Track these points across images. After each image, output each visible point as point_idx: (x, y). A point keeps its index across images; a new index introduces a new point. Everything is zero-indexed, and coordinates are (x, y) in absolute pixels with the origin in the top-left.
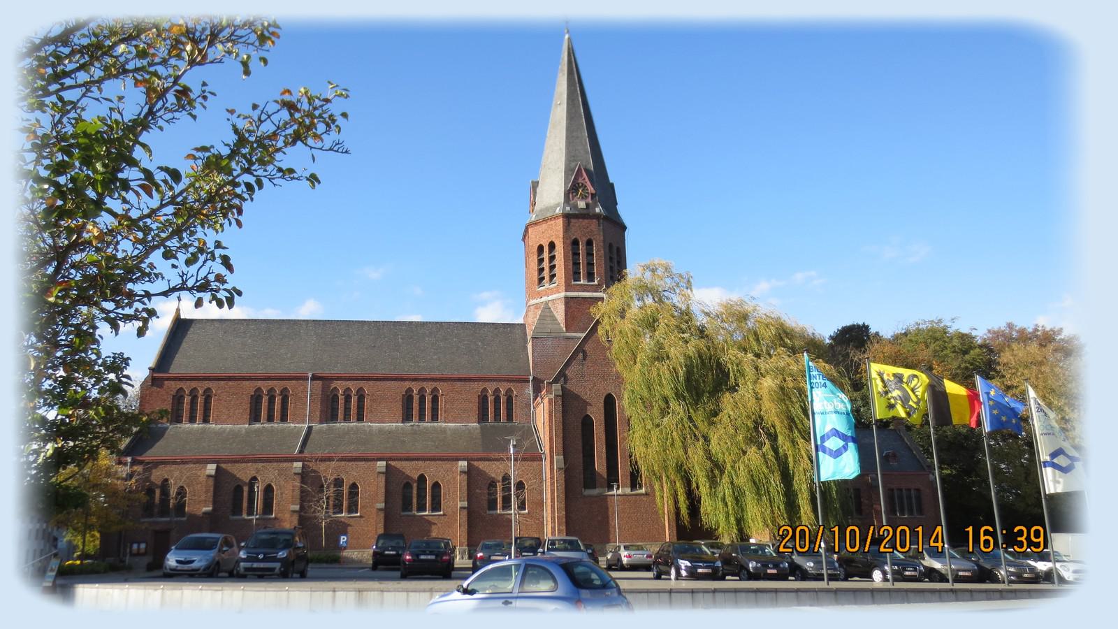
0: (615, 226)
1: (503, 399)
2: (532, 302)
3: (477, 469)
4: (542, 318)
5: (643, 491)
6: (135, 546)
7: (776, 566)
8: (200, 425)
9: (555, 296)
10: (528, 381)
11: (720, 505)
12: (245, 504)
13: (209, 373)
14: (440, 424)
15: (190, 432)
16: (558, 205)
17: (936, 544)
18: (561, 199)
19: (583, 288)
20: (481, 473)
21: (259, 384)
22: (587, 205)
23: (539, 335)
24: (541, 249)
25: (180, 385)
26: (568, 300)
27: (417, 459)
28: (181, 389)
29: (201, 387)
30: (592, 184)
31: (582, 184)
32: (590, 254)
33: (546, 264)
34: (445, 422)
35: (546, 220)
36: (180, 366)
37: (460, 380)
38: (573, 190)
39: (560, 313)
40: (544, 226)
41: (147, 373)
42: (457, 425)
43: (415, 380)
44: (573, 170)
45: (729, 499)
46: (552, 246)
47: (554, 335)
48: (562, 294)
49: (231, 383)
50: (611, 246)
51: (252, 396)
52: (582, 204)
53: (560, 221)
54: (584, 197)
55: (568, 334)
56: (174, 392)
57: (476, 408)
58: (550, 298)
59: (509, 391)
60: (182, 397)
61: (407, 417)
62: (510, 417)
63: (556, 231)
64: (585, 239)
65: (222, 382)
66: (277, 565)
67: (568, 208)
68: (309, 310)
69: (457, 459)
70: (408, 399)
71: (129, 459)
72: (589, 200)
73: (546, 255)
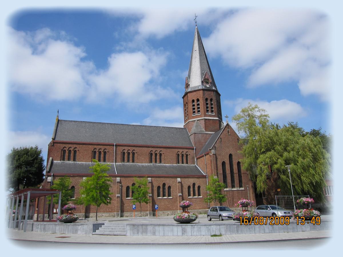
5: (171, 197)
8: (72, 162)
16: (200, 86)
17: (313, 222)
18: (200, 84)
19: (210, 116)
21: (95, 146)
31: (207, 79)
33: (196, 107)
34: (165, 163)
40: (195, 93)
46: (198, 100)
50: (217, 101)
51: (92, 151)
65: (81, 145)
73: (209, 102)
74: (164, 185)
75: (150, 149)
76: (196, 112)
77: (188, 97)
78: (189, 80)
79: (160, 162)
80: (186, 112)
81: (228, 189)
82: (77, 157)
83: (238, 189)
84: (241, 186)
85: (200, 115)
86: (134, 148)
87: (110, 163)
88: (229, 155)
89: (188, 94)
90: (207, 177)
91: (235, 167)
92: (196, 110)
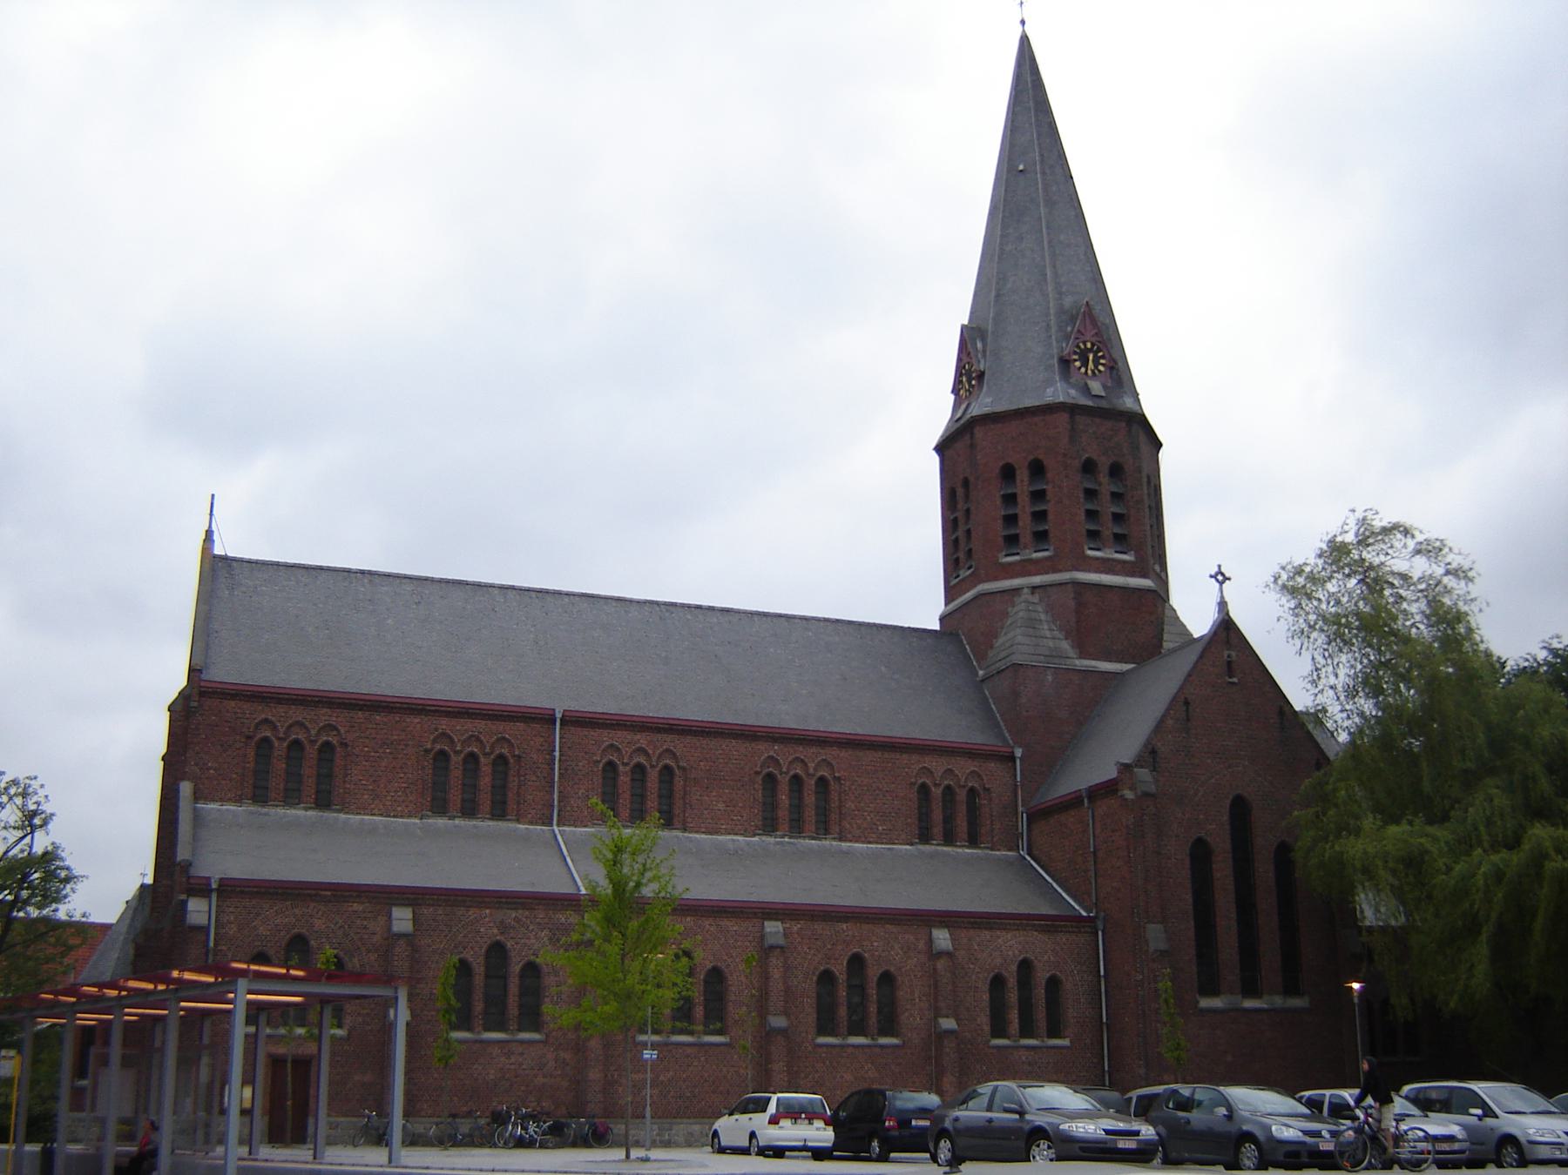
8: (310, 813)
33: (1024, 508)
46: (1037, 469)
74: (857, 963)
75: (762, 746)
76: (1026, 537)
77: (972, 446)
78: (979, 345)
80: (960, 533)
81: (1216, 1003)
83: (1278, 1001)
84: (1054, 1032)
85: (1047, 558)
86: (669, 738)
87: (531, 823)
88: (1228, 802)
89: (979, 432)
90: (1100, 925)
91: (1264, 871)
92: (1025, 526)
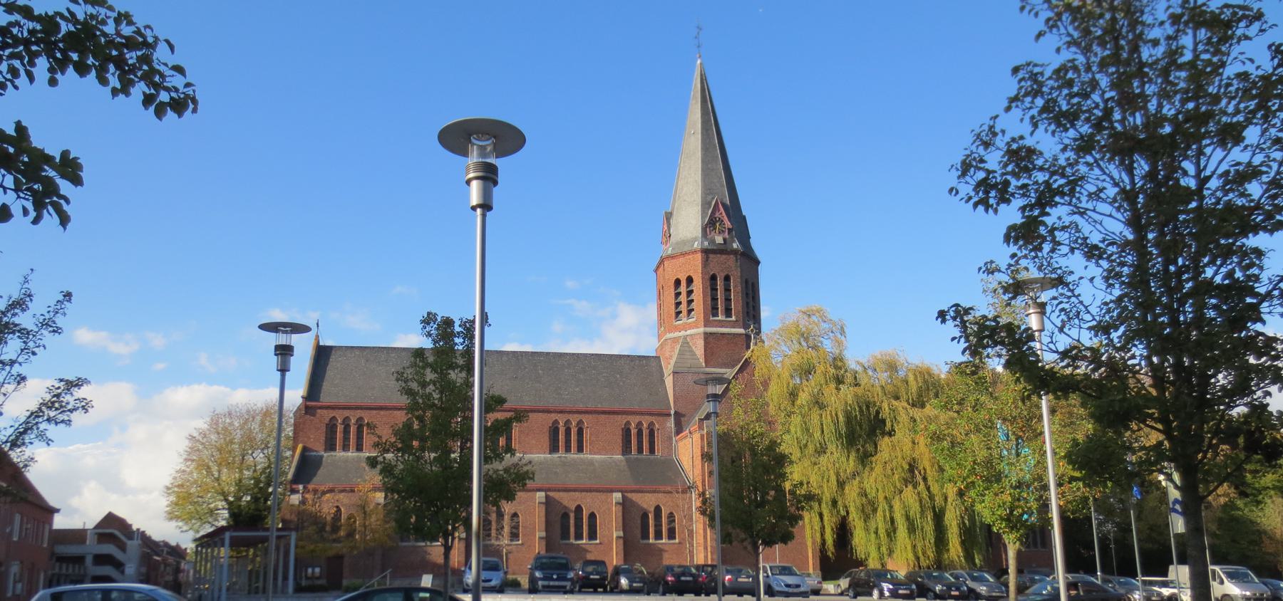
0: (750, 260)
1: (645, 432)
2: (669, 335)
3: (631, 501)
4: (681, 353)
6: (310, 570)
7: (958, 589)
9: (694, 330)
10: (669, 415)
11: (873, 536)
12: (572, 530)
13: (359, 402)
14: (586, 456)
15: (346, 461)
16: (695, 239)
18: (699, 233)
19: (722, 324)
20: (633, 504)
22: (725, 240)
23: (679, 370)
24: (678, 282)
25: (332, 413)
26: (707, 336)
27: (575, 490)
28: (334, 418)
29: (353, 417)
30: (727, 214)
32: (727, 290)
33: (683, 298)
35: (684, 254)
36: (329, 394)
37: (604, 412)
38: (711, 224)
39: (699, 348)
40: (681, 260)
41: (300, 401)
42: (602, 456)
43: (561, 412)
44: (710, 203)
45: (882, 532)
46: (690, 280)
47: (693, 370)
48: (702, 330)
49: (382, 412)
50: (747, 282)
52: (719, 240)
53: (699, 256)
54: (721, 232)
55: (708, 370)
56: (327, 421)
57: (620, 441)
58: (689, 332)
59: (651, 424)
60: (335, 426)
61: (554, 448)
62: (652, 451)
63: (694, 266)
64: (723, 275)
66: (568, 584)
67: (706, 243)
68: (528, 348)
69: (612, 491)
70: (554, 431)
71: (301, 487)
72: (726, 235)
73: (683, 289)
79: (580, 449)
82: (665, 411)
